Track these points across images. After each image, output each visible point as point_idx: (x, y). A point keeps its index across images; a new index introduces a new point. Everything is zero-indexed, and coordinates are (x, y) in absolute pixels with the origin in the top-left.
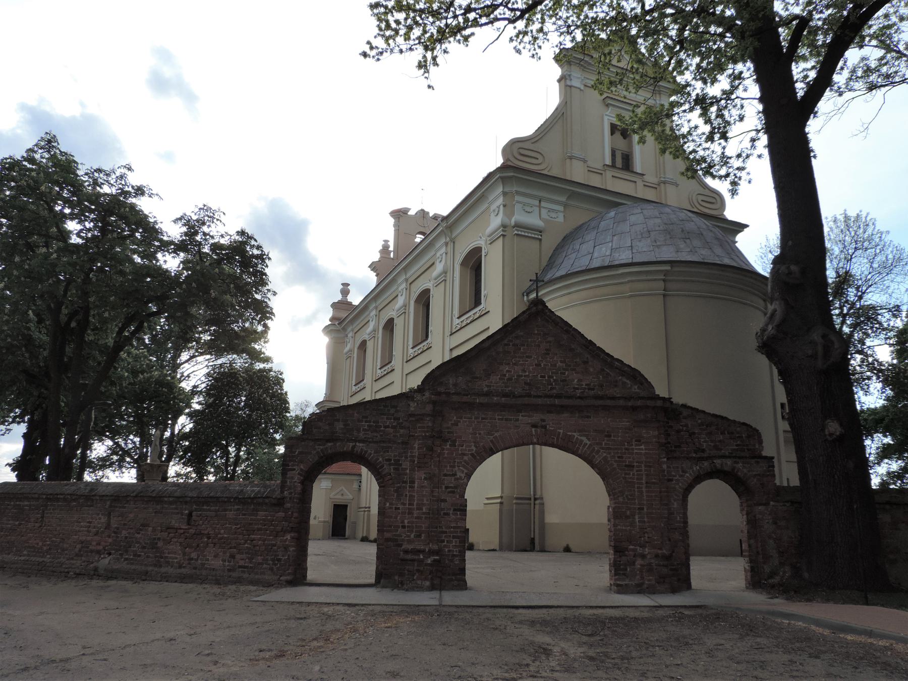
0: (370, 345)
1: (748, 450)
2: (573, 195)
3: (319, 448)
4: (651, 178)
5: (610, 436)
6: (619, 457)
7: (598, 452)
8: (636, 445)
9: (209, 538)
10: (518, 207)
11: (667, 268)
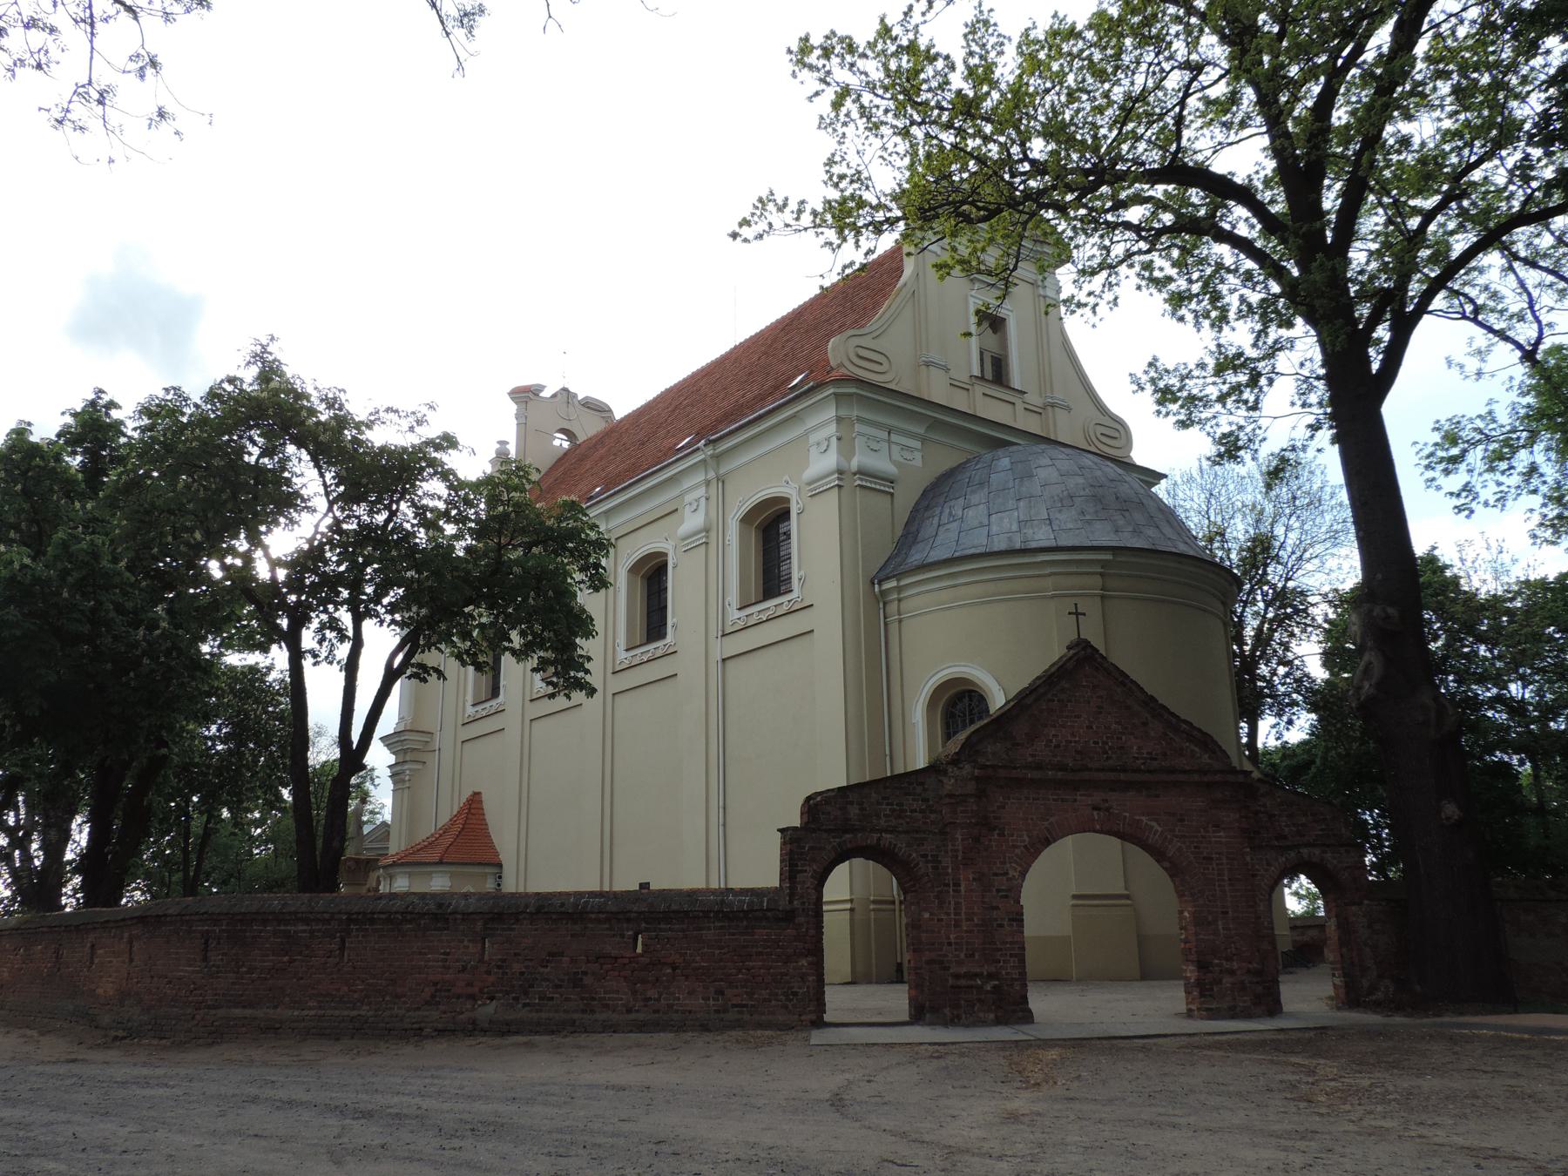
2: (935, 425)
4: (1034, 398)
9: (674, 969)
10: (859, 443)
11: (1108, 556)
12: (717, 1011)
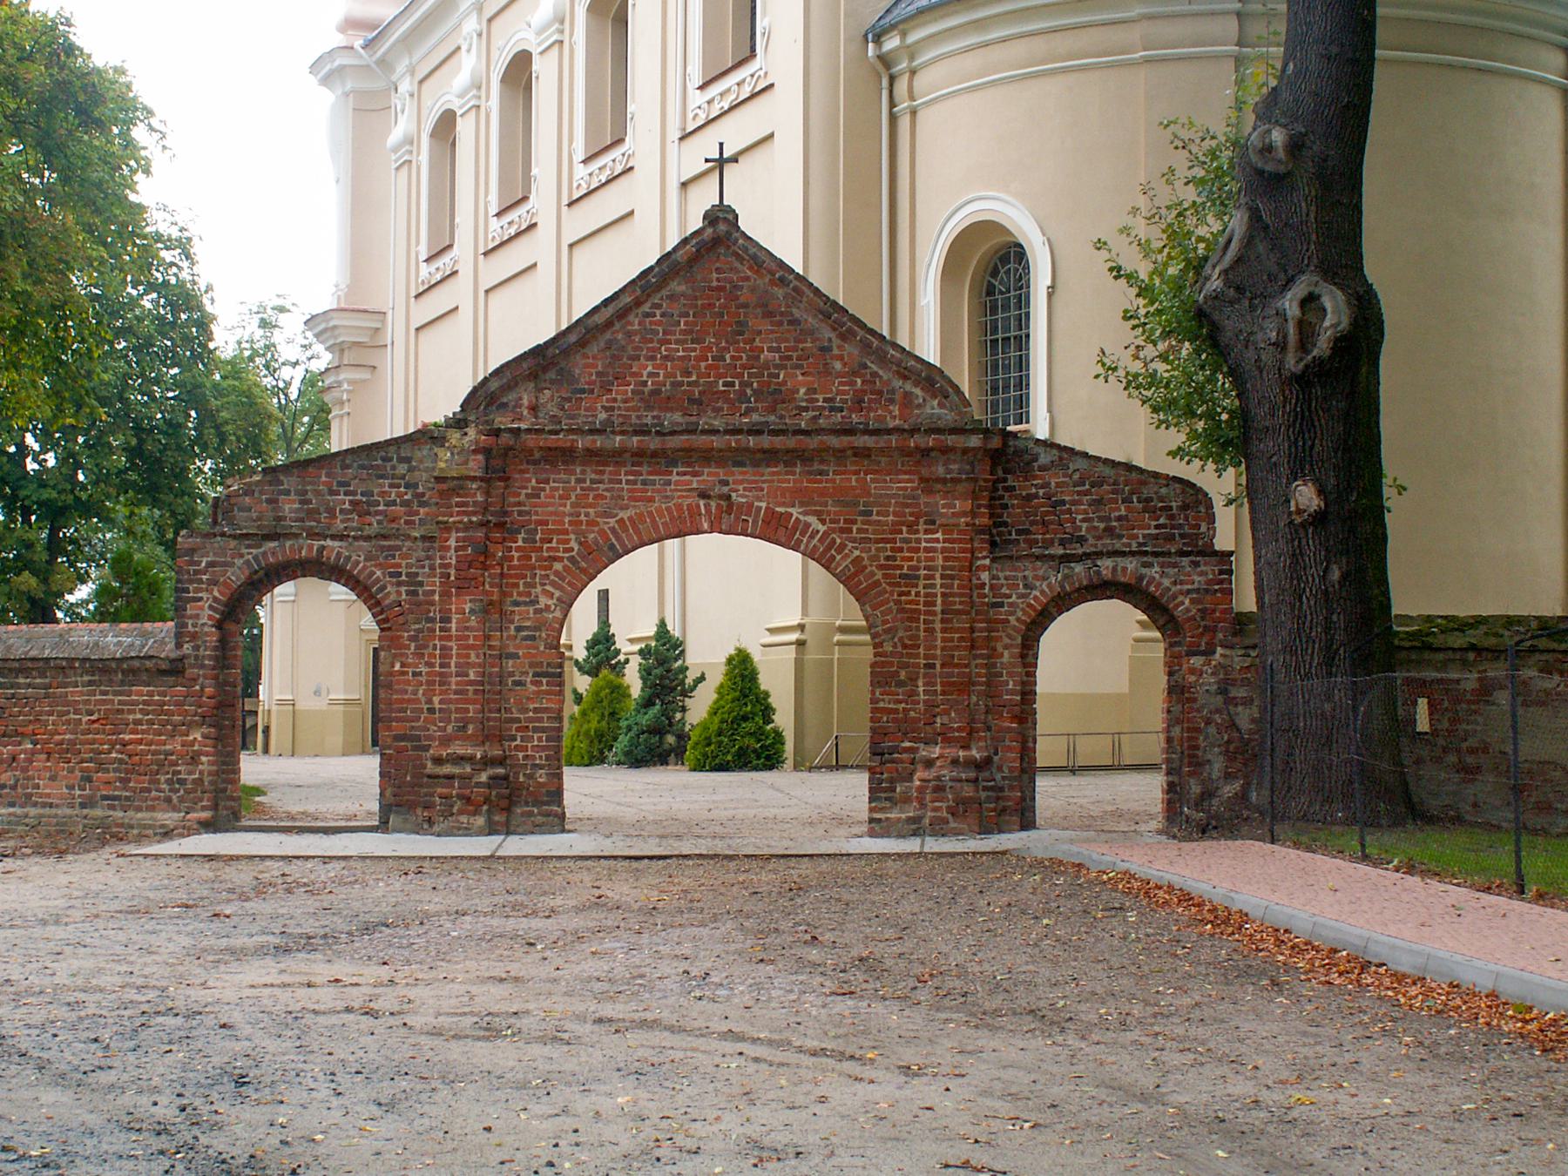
0: (465, 129)
1: (1182, 536)
3: (250, 553)
5: (870, 513)
6: (887, 558)
7: (842, 546)
8: (926, 532)
12: (83, 806)
